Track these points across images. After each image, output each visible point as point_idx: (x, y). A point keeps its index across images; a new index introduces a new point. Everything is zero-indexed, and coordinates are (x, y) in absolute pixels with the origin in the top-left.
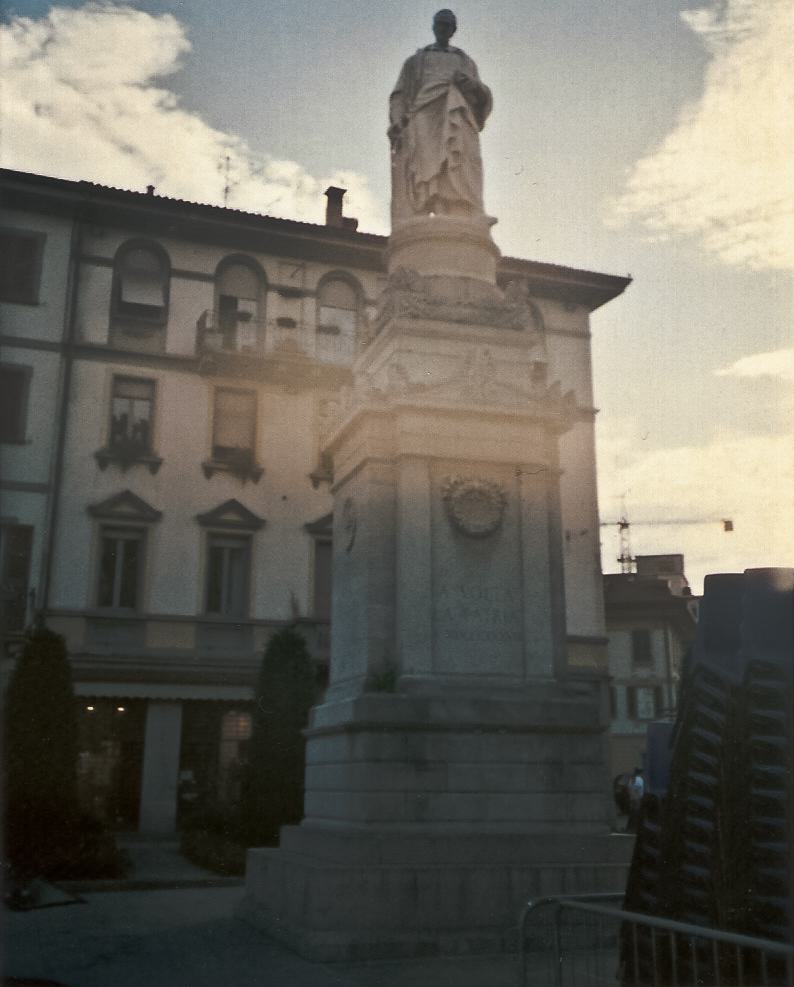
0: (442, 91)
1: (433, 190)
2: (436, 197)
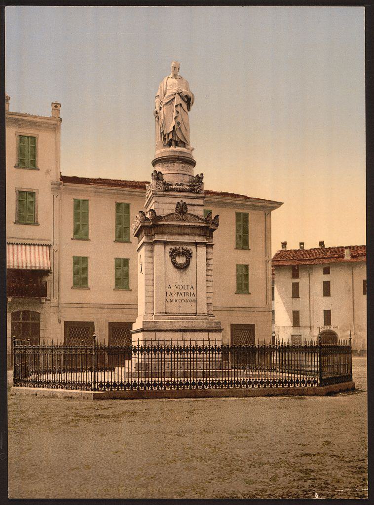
0: (173, 97)
1: (171, 137)
2: (171, 140)
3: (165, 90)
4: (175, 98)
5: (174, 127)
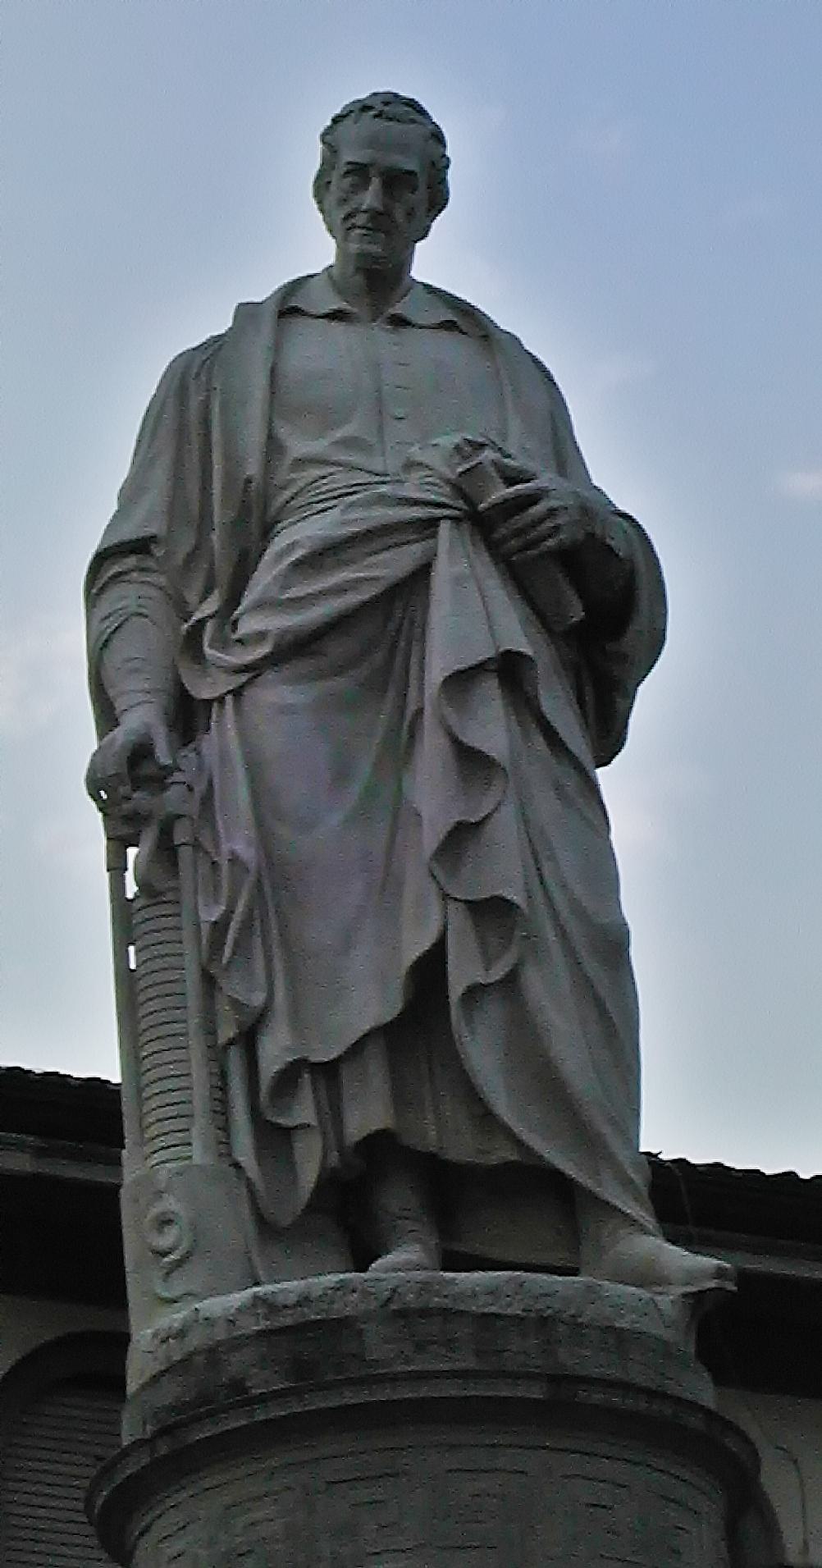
0: (393, 564)
2: (378, 1144)
3: (253, 468)
4: (423, 573)
5: (430, 969)
